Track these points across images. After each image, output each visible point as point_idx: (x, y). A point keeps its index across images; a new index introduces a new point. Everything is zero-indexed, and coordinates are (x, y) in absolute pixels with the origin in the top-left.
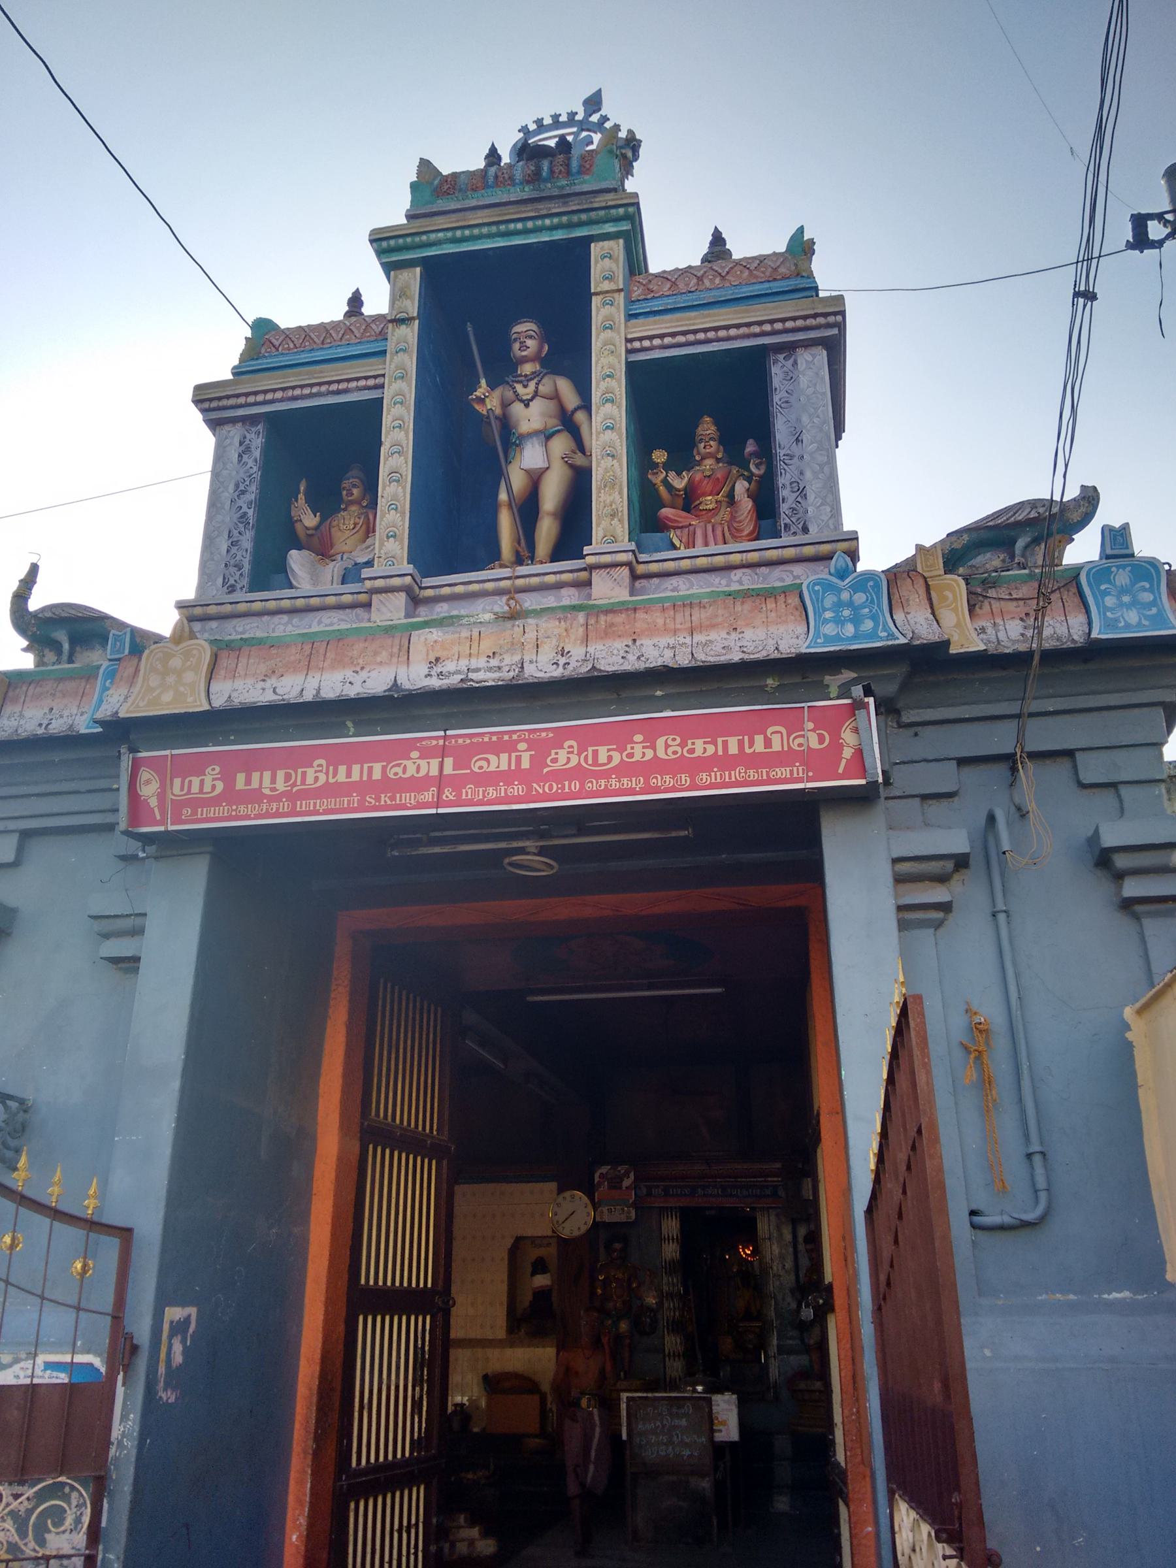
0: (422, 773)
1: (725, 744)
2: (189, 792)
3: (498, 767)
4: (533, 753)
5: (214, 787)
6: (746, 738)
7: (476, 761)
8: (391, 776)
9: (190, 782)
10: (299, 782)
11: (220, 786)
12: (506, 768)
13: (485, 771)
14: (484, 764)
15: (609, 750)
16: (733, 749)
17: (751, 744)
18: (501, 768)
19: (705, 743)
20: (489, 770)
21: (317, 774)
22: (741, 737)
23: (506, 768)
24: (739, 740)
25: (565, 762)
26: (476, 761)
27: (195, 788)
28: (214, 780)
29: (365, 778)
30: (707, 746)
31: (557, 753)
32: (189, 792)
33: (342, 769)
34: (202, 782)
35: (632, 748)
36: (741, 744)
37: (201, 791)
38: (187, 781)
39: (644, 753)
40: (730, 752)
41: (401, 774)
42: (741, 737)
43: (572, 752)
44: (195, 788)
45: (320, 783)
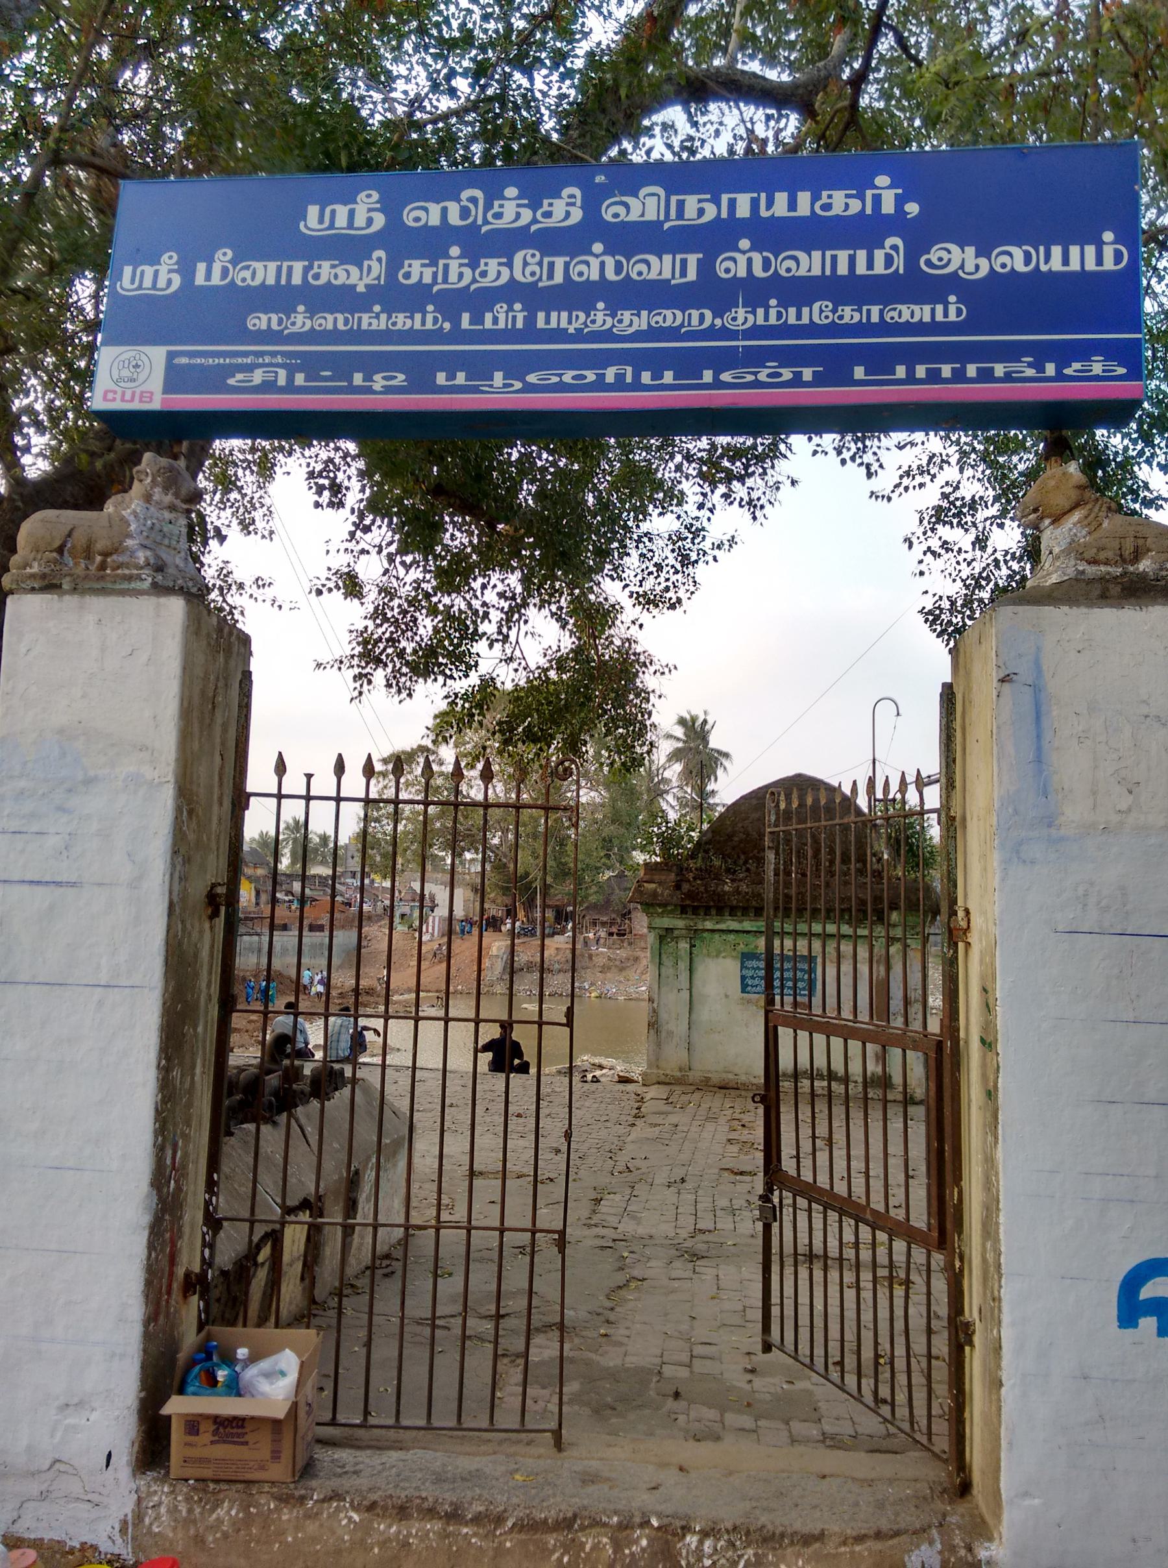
0: (916, 319)
1: (732, 203)
2: (332, 226)
3: (643, 215)
4: (900, 191)
5: (370, 221)
6: (763, 196)
7: (608, 207)
8: (889, 320)
9: (333, 212)
10: (545, 277)
11: (380, 220)
12: (819, 273)
13: (344, 285)
14: (621, 210)
15: (700, 201)
16: (875, 318)
17: (770, 204)
18: (812, 273)
19: (847, 196)
20: (648, 278)
21: (701, 205)
22: (755, 195)
23: (819, 273)
24: (752, 198)
25: (562, 217)
26: (608, 207)
27: (341, 221)
28: (370, 210)
29: (828, 272)
30: (850, 201)
31: (830, 197)
32: (140, 287)
33: (781, 198)
34: (352, 214)
35: (501, 206)
36: (755, 203)
37: (154, 287)
38: (328, 210)
39: (847, 205)
40: (839, 273)
41: (896, 318)
42: (755, 195)
43: (573, 204)
44: (341, 221)
45: (749, 324)
